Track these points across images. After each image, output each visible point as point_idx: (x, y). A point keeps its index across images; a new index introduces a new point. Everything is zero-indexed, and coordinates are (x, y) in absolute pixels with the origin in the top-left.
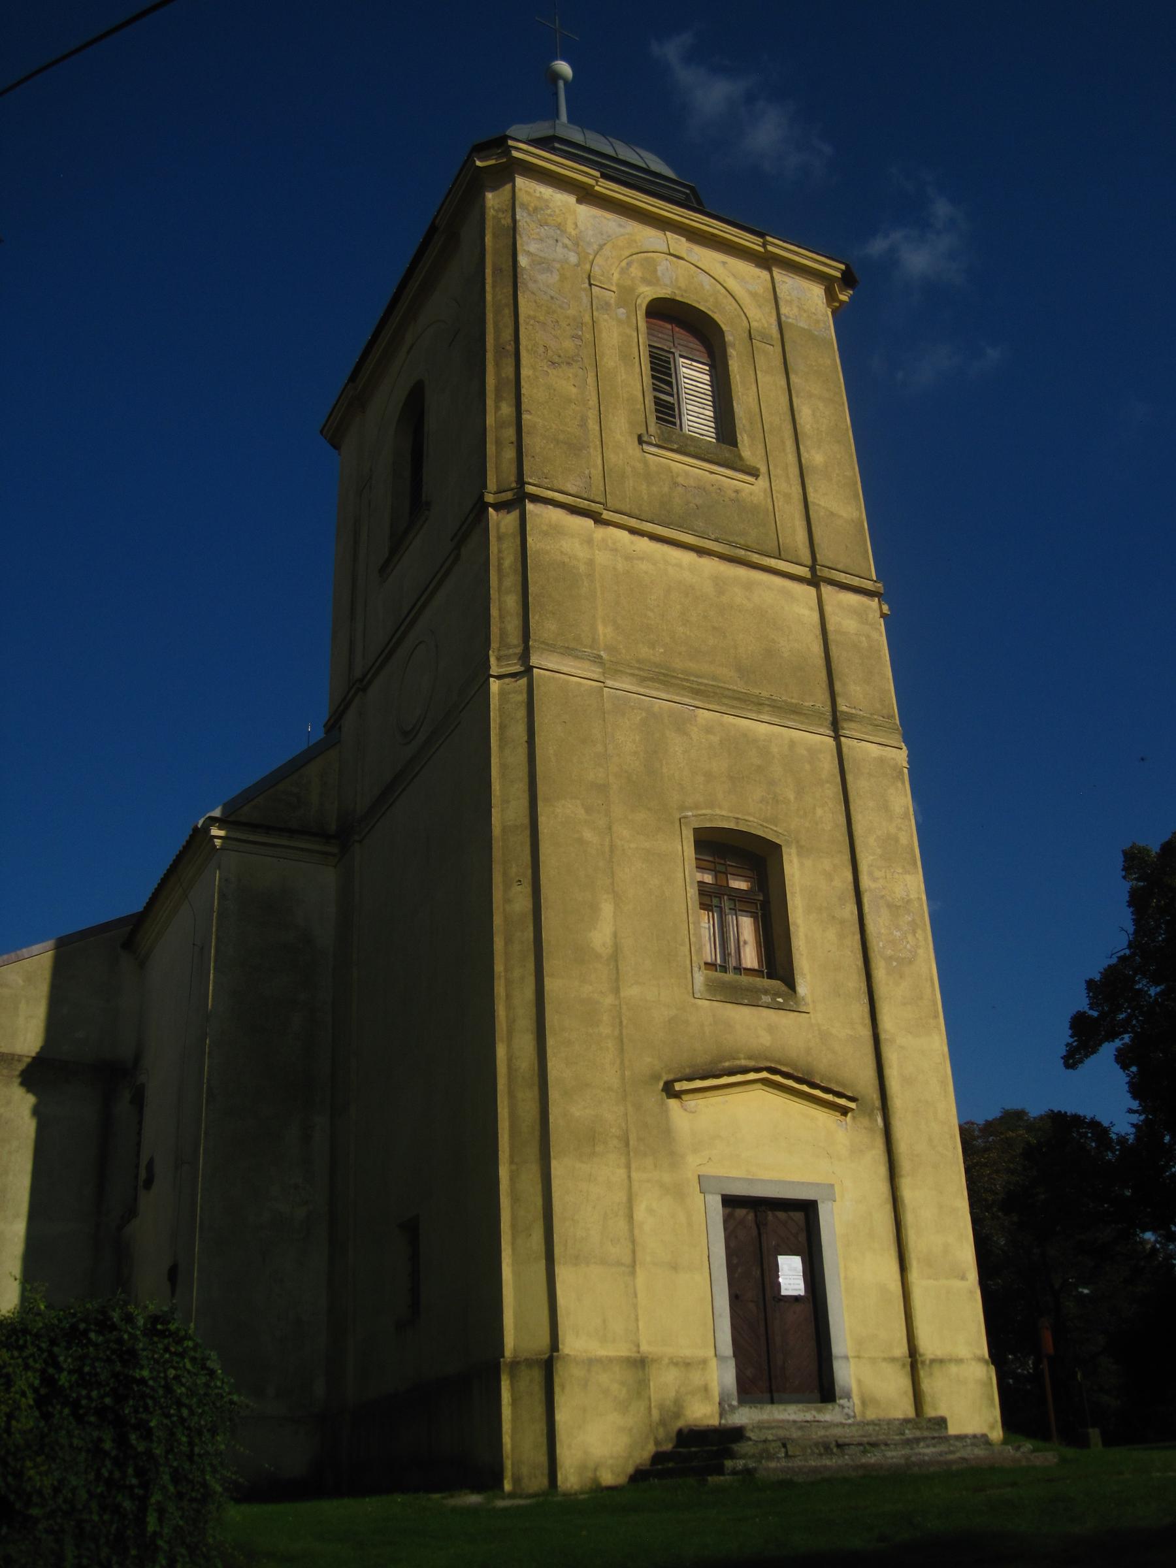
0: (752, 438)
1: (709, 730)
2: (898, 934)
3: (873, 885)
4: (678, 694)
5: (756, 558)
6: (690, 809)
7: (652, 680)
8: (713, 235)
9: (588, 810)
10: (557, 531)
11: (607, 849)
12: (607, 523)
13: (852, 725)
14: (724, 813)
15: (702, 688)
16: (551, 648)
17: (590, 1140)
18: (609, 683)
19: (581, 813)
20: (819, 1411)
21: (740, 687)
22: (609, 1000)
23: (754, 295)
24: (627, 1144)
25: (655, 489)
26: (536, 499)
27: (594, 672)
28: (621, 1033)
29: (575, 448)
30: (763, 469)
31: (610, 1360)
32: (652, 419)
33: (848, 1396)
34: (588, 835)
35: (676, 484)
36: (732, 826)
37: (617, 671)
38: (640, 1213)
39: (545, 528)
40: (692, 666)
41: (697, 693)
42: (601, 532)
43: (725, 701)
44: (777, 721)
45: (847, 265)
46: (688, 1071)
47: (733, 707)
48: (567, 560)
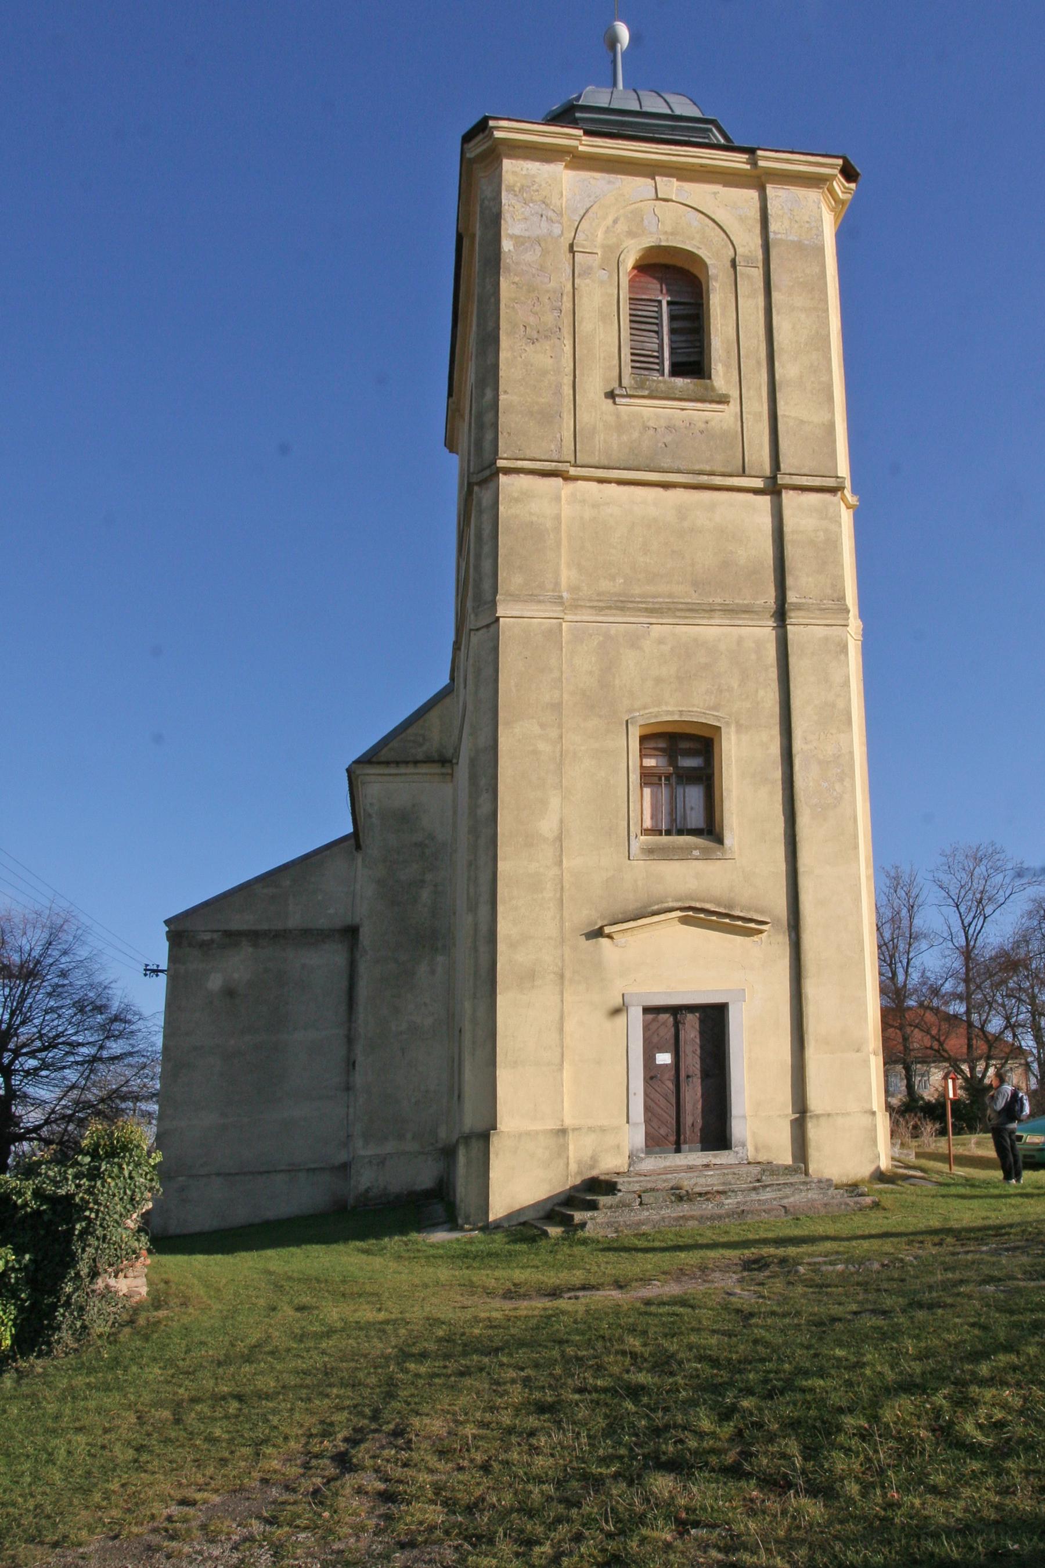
0: (727, 366)
1: (661, 641)
2: (826, 784)
3: (806, 747)
4: (633, 616)
5: (718, 481)
6: (639, 710)
7: (609, 608)
8: (702, 165)
9: (542, 726)
10: (526, 496)
11: (558, 755)
12: (576, 479)
13: (801, 613)
14: (670, 709)
15: (657, 606)
16: (516, 598)
17: (529, 977)
18: (568, 617)
19: (537, 730)
20: (715, 1156)
21: (694, 598)
22: (554, 871)
23: (742, 219)
24: (562, 976)
25: (625, 438)
26: (508, 471)
27: (555, 611)
28: (562, 896)
29: (547, 417)
30: (734, 394)
31: (537, 1132)
32: (627, 371)
33: (744, 1145)
34: (542, 746)
35: (646, 428)
36: (676, 718)
37: (576, 607)
38: (569, 1026)
39: (516, 495)
40: (650, 589)
41: (651, 611)
42: (571, 486)
43: (678, 614)
44: (728, 622)
45: (845, 159)
46: (620, 916)
47: (687, 617)
48: (535, 519)
